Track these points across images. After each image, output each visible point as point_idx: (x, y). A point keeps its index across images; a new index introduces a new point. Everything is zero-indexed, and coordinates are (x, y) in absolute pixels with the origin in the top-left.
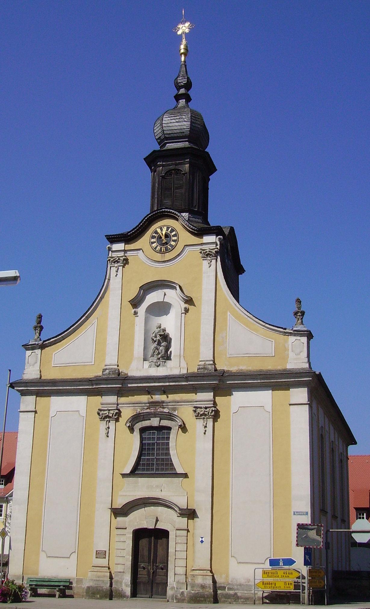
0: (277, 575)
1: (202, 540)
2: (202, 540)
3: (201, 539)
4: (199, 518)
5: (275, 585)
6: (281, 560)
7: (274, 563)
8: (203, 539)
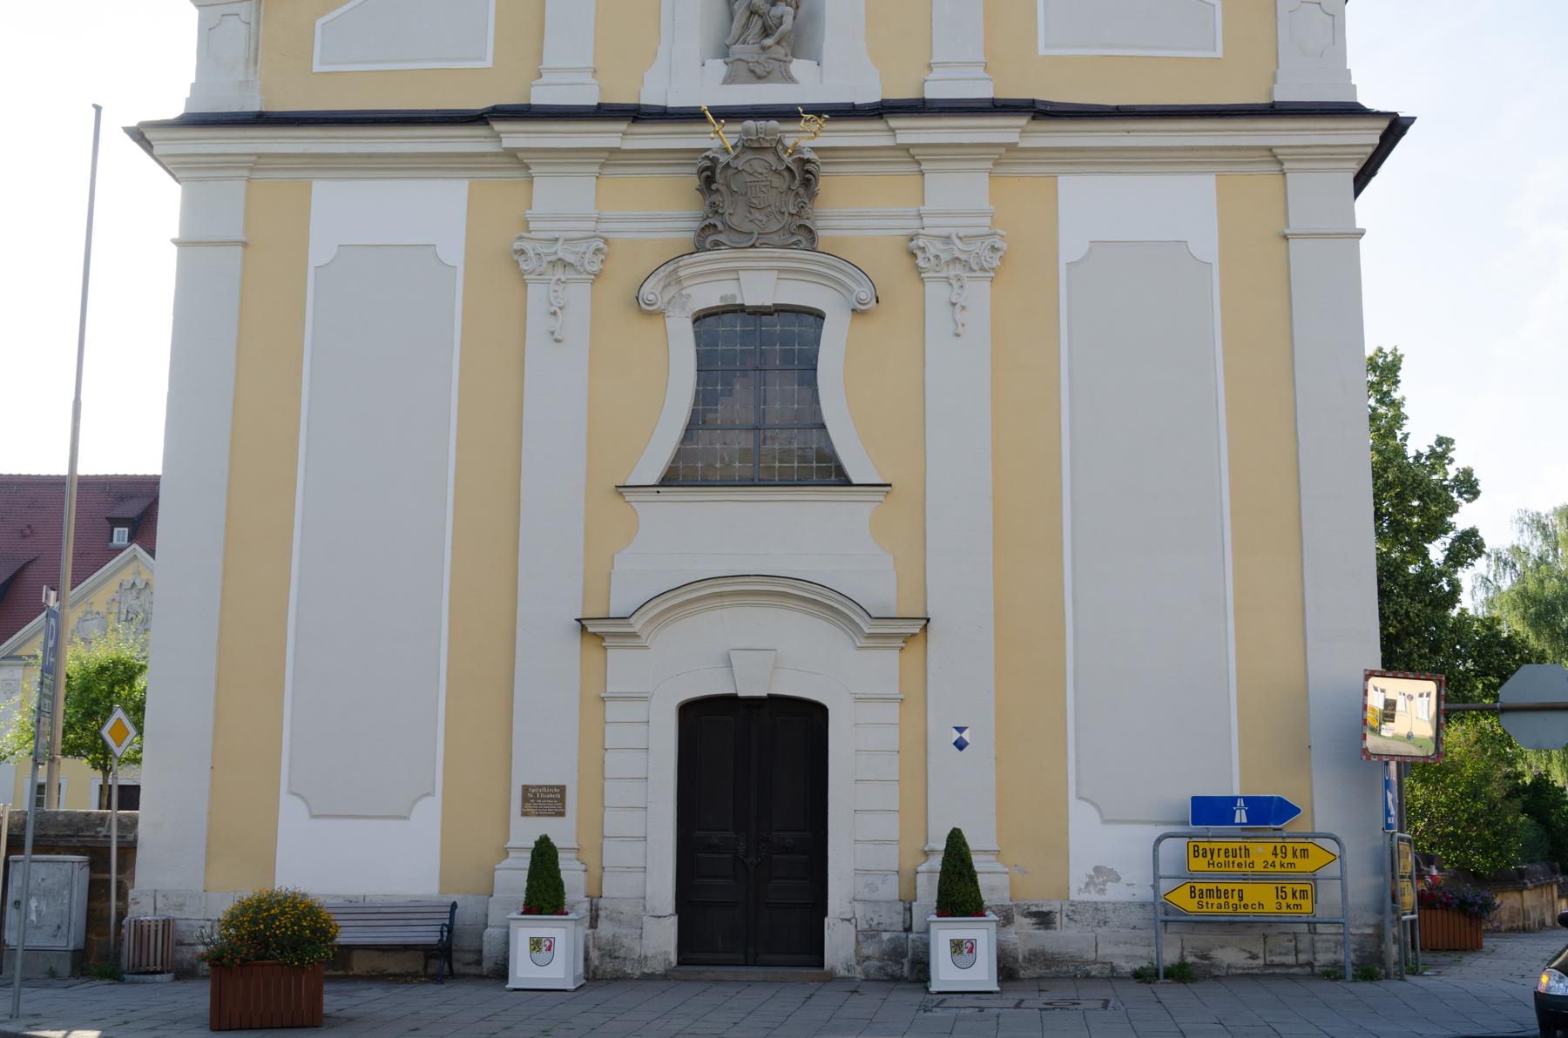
0: (1249, 861)
1: (961, 738)
2: (961, 738)
3: (956, 735)
4: (1415, 118)
5: (1241, 898)
6: (1240, 803)
7: (1209, 810)
8: (966, 735)
